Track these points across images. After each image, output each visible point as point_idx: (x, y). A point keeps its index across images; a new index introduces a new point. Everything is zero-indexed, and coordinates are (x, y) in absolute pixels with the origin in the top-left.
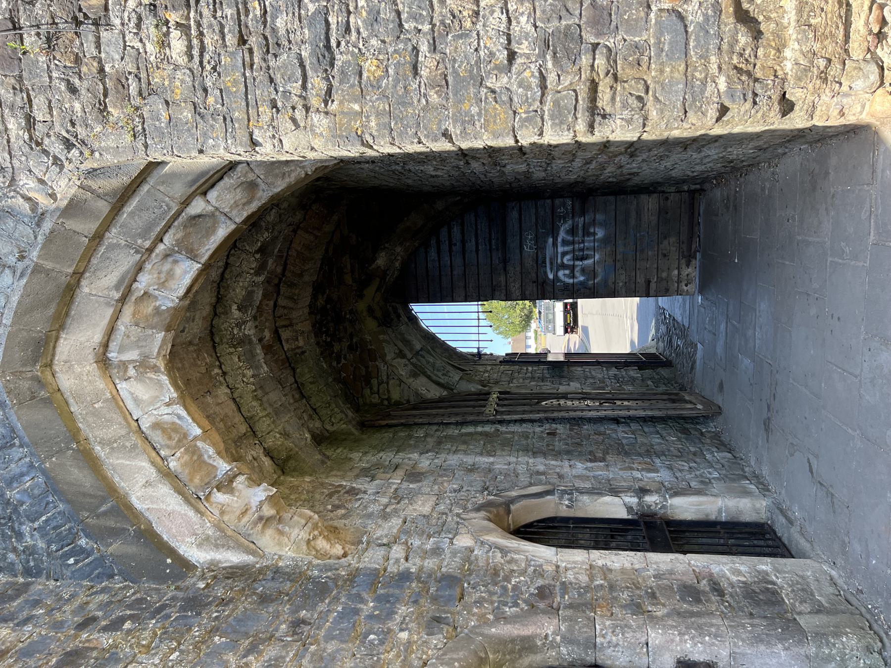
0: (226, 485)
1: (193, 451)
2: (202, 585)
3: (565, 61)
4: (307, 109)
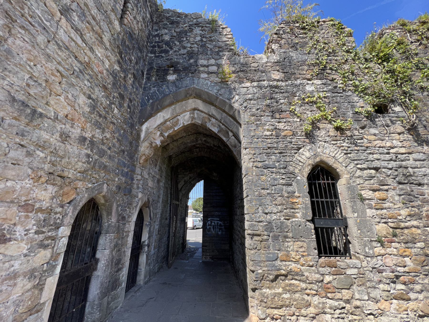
0: (162, 135)
1: (171, 128)
2: (136, 128)
3: (265, 228)
4: (254, 162)
